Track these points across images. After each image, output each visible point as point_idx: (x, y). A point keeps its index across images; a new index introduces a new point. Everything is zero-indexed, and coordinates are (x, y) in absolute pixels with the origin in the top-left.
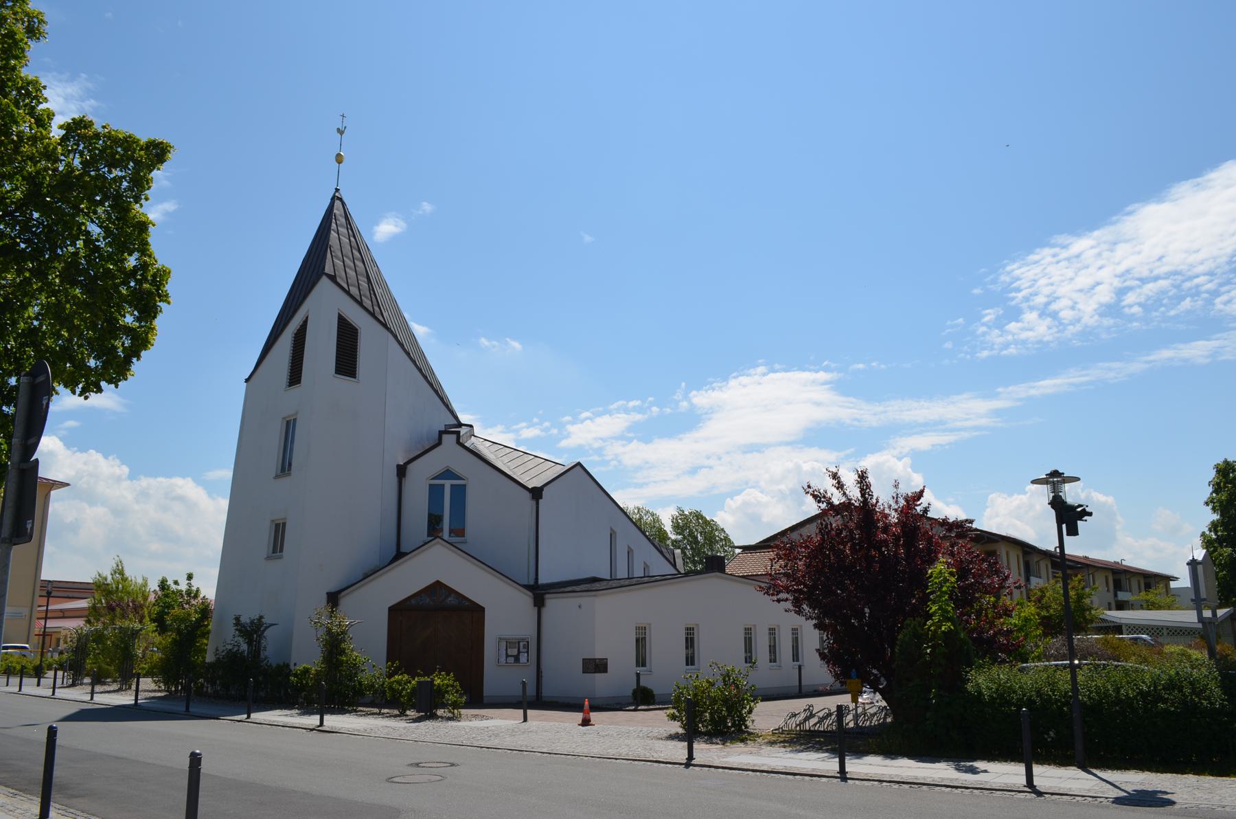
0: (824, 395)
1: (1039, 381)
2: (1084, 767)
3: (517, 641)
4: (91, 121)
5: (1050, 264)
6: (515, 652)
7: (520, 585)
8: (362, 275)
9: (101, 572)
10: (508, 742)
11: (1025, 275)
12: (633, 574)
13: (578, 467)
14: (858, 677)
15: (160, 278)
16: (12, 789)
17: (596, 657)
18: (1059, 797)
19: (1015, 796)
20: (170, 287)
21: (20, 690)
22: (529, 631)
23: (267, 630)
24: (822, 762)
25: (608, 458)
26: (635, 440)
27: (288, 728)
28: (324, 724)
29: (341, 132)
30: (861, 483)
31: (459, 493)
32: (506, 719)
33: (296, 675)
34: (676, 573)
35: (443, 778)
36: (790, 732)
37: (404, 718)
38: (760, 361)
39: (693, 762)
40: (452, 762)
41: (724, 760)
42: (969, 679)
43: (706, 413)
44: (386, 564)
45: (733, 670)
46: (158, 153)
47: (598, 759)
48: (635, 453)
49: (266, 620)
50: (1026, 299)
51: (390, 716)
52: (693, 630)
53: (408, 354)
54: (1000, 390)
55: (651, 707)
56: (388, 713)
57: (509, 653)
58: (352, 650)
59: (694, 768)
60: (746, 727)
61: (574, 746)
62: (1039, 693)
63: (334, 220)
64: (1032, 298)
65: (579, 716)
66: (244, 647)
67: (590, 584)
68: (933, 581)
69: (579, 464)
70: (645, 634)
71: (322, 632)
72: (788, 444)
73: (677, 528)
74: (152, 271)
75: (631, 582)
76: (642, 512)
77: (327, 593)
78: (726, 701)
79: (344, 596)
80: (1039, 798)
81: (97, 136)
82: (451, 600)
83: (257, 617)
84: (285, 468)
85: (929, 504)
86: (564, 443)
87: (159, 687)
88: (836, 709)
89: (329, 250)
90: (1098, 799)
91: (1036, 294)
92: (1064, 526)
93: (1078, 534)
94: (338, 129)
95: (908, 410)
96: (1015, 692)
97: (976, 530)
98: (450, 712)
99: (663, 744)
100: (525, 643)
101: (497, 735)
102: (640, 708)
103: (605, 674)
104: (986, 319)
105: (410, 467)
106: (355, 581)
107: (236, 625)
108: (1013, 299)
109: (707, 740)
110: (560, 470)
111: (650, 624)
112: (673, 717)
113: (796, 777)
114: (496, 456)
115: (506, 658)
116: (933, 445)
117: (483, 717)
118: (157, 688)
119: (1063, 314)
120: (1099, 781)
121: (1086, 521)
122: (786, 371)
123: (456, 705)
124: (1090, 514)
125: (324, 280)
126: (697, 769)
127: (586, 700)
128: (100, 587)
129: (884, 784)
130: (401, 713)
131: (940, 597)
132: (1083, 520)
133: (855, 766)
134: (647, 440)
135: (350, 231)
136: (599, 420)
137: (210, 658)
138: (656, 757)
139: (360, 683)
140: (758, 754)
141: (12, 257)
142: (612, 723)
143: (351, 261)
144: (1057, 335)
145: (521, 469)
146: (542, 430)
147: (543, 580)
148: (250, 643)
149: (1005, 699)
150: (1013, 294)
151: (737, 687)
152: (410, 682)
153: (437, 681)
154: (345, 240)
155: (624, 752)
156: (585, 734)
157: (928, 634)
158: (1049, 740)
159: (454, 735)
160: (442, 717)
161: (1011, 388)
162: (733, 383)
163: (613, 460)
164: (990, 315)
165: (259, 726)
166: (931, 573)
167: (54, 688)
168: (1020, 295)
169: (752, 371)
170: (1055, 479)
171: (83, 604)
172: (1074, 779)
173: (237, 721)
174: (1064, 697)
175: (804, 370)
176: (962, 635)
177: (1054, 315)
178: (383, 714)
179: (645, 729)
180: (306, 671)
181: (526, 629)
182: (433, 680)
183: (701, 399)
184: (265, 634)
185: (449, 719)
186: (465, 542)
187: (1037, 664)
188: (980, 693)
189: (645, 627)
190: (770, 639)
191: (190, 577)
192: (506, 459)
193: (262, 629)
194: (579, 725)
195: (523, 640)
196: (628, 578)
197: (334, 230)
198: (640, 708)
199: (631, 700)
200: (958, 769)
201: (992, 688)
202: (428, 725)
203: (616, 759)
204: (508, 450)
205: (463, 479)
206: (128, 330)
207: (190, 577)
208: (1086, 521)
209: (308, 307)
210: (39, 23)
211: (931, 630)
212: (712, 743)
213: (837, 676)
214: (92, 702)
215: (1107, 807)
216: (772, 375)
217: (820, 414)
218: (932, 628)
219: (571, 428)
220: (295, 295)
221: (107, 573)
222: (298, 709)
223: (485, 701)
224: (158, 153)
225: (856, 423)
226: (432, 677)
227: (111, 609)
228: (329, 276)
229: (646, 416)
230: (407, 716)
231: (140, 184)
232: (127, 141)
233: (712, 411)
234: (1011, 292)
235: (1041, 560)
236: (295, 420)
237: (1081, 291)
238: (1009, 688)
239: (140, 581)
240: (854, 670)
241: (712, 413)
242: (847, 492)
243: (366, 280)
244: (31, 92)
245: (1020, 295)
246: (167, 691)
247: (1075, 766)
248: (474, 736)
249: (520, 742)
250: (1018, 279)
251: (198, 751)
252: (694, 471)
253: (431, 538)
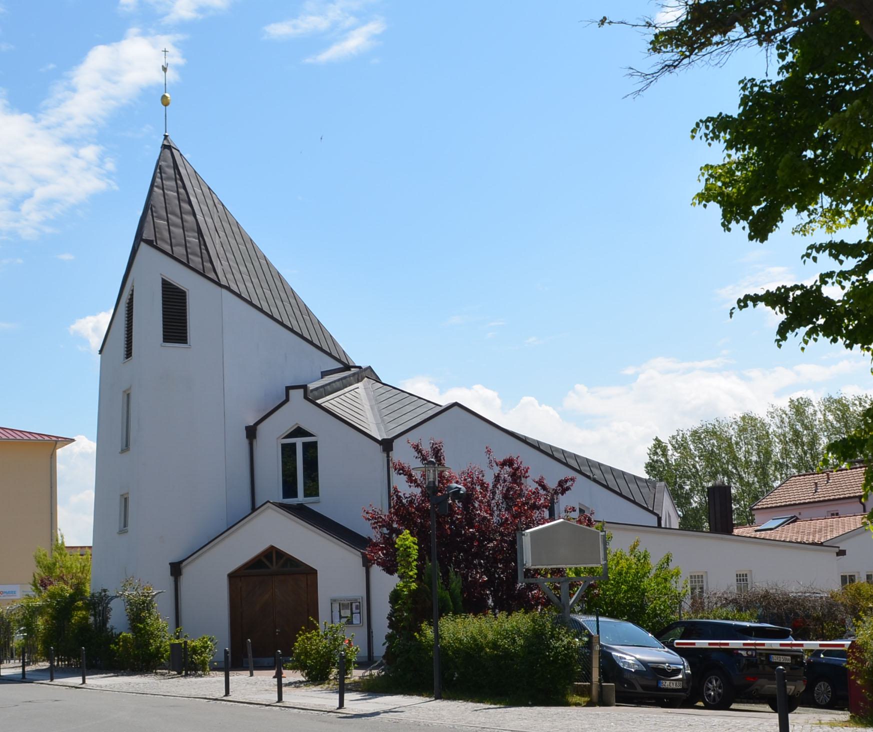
3: (349, 602)
22: (360, 592)
28: (283, 700)
31: (311, 449)
52: (746, 576)
57: (343, 615)
76: (865, 402)
77: (170, 564)
79: (186, 565)
89: (150, 211)
105: (260, 427)
111: (751, 571)
195: (356, 601)
205: (314, 436)
243: (196, 235)
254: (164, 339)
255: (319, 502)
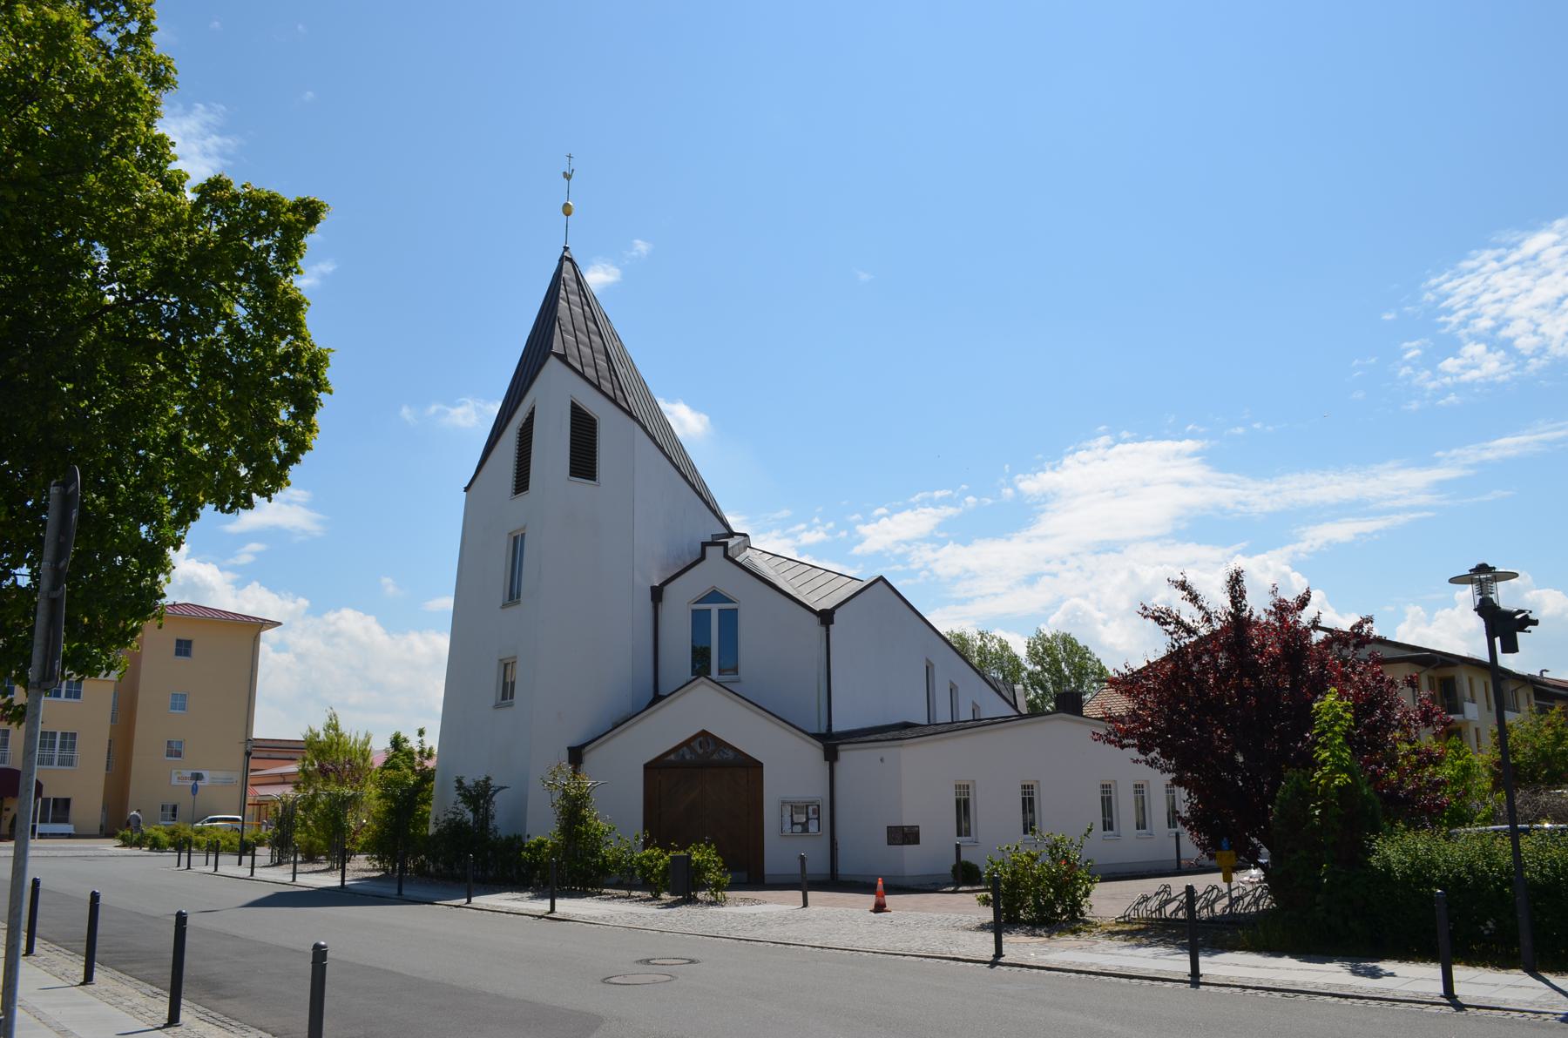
0: (1193, 471)
1: (1495, 440)
2: (1533, 971)
4: (229, 181)
5: (1495, 272)
7: (808, 734)
8: (600, 352)
9: (312, 728)
10: (775, 933)
11: (1457, 291)
12: (935, 719)
13: (881, 582)
14: (1231, 848)
15: (318, 361)
16: (157, 987)
17: (904, 825)
18: (1487, 1011)
19: (1426, 1010)
20: (329, 374)
21: (216, 870)
22: (819, 792)
23: (501, 791)
24: (1176, 963)
25: (914, 567)
26: (951, 543)
27: (512, 915)
28: (556, 910)
29: (567, 176)
30: (1233, 587)
31: (730, 619)
32: (782, 903)
33: (529, 850)
34: (1017, 714)
35: (673, 977)
36: (1139, 920)
37: (657, 902)
38: (1102, 428)
39: (1002, 960)
40: (689, 957)
41: (1045, 957)
42: (1375, 850)
43: (1038, 503)
44: (644, 707)
45: (1062, 840)
46: (310, 212)
47: (881, 956)
48: (953, 559)
49: (494, 782)
50: (1464, 324)
51: (640, 900)
53: (661, 449)
54: (1439, 454)
55: (976, 888)
56: (639, 896)
58: (596, 819)
59: (1002, 968)
60: (1082, 914)
61: (855, 938)
62: (1470, 867)
63: (562, 287)
64: (1472, 322)
65: (871, 900)
66: (469, 816)
67: (901, 731)
68: (1321, 718)
69: (881, 579)
70: (968, 795)
71: (557, 795)
72: (1156, 538)
73: (1033, 654)
74: (306, 356)
75: (955, 727)
76: (986, 638)
77: (568, 748)
78: (1053, 880)
80: (1459, 1013)
81: (236, 198)
82: (731, 754)
83: (483, 778)
84: (513, 596)
85: (1319, 613)
86: (857, 550)
87: (374, 866)
88: (1184, 890)
89: (557, 323)
90: (1542, 1015)
91: (1477, 316)
92: (1497, 640)
93: (1517, 651)
94: (565, 173)
95: (1313, 487)
96: (1437, 867)
97: (1381, 641)
98: (712, 894)
99: (969, 936)
100: (816, 807)
101: (763, 925)
102: (961, 889)
103: (915, 846)
104: (1409, 355)
105: (668, 588)
106: (602, 733)
107: (458, 788)
108: (1445, 324)
109: (1028, 931)
110: (857, 586)
112: (985, 901)
113: (1132, 981)
114: (776, 571)
115: (792, 826)
116: (1357, 535)
117: (754, 901)
118: (371, 867)
119: (1520, 343)
120: (1550, 990)
121: (1530, 632)
122: (1140, 440)
123: (719, 886)
124: (1535, 623)
125: (553, 360)
126: (1005, 969)
127: (880, 879)
128: (311, 747)
129: (1249, 991)
130: (654, 896)
131: (1332, 739)
132: (1525, 631)
133: (1216, 966)
134: (965, 542)
135: (583, 299)
136: (897, 517)
137: (432, 830)
138: (956, 953)
139: (604, 858)
140: (1091, 950)
141: (142, 348)
142: (916, 909)
143: (584, 334)
144: (1514, 373)
145: (807, 588)
146: (827, 533)
147: (837, 727)
148: (475, 811)
149: (1424, 876)
150: (1443, 319)
151: (1068, 862)
152: (663, 857)
153: (696, 857)
154: (577, 310)
155: (916, 946)
156: (875, 922)
157: (1317, 790)
158: (1486, 932)
159: (710, 924)
160: (701, 902)
161: (1455, 452)
162: (1067, 461)
163: (921, 570)
164: (1413, 351)
165: (480, 912)
166: (1318, 707)
167: (253, 868)
168: (1455, 319)
169: (1092, 444)
170: (1483, 576)
171: (293, 768)
172: (1515, 987)
173: (455, 906)
174: (1506, 875)
175: (1164, 438)
176: (1365, 791)
177: (1508, 345)
178: (633, 897)
179: (953, 916)
180: (541, 845)
181: (815, 790)
182: (690, 855)
183: (1030, 485)
184: (493, 800)
185: (711, 903)
186: (738, 681)
187: (1468, 829)
188: (1389, 869)
189: (1032, 786)
190: (1168, 798)
191: (421, 733)
192: (789, 575)
193: (490, 793)
194: (871, 911)
195: (812, 803)
196: (974, 720)
197: (563, 299)
198: (961, 889)
199: (951, 880)
200: (1355, 972)
201: (1406, 862)
202: (685, 910)
203: (904, 955)
204: (792, 564)
206: (285, 433)
207: (421, 733)
208: (1530, 632)
209: (536, 394)
210: (167, 69)
211: (1321, 785)
212: (1034, 935)
213: (1202, 846)
214: (294, 883)
215: (1551, 1027)
216: (1120, 448)
217: (1192, 497)
218: (1322, 782)
219: (863, 529)
220: (519, 382)
221: (319, 728)
222: (532, 892)
223: (767, 881)
224: (310, 212)
225: (1241, 508)
226: (688, 851)
227: (324, 772)
228: (557, 356)
229: (961, 510)
230: (661, 899)
231: (289, 251)
232: (270, 202)
233: (1047, 499)
234: (1440, 316)
235: (1520, 688)
236: (523, 535)
237: (1543, 306)
238: (1429, 861)
239: (361, 738)
240: (1225, 839)
241: (1046, 502)
242: (1204, 605)
243: (604, 358)
244: (157, 150)
245: (1455, 319)
246: (383, 870)
247: (1521, 968)
248: (735, 924)
249: (790, 933)
250: (1447, 296)
251: (323, 943)
252: (1032, 580)
253: (694, 677)
254: (571, 471)
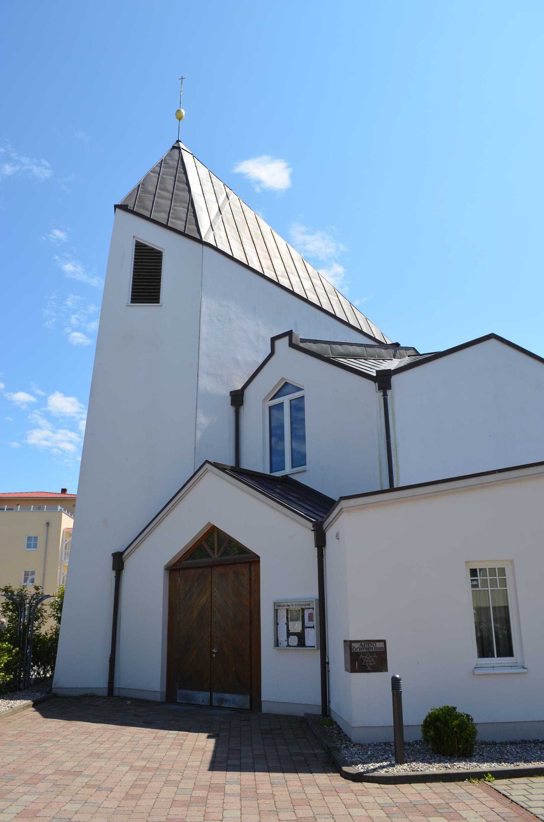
3: (299, 608)
6: (296, 627)
105: (247, 391)
115: (288, 637)
255: (305, 471)
